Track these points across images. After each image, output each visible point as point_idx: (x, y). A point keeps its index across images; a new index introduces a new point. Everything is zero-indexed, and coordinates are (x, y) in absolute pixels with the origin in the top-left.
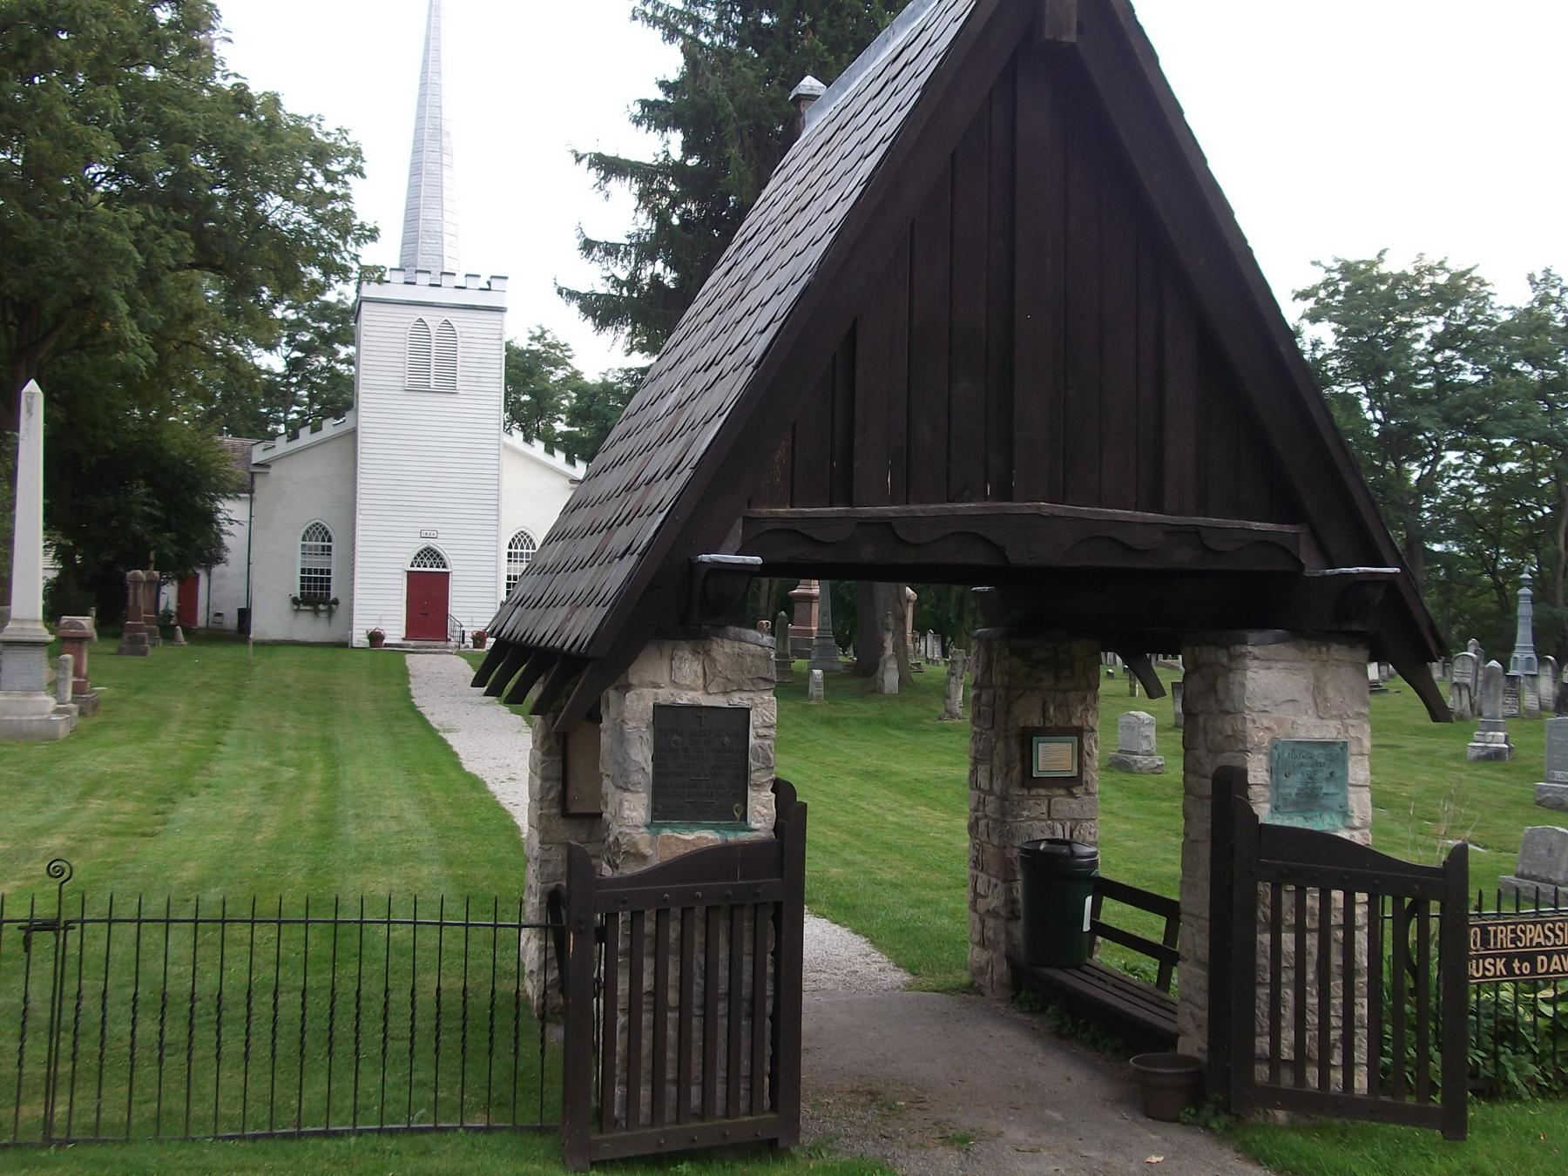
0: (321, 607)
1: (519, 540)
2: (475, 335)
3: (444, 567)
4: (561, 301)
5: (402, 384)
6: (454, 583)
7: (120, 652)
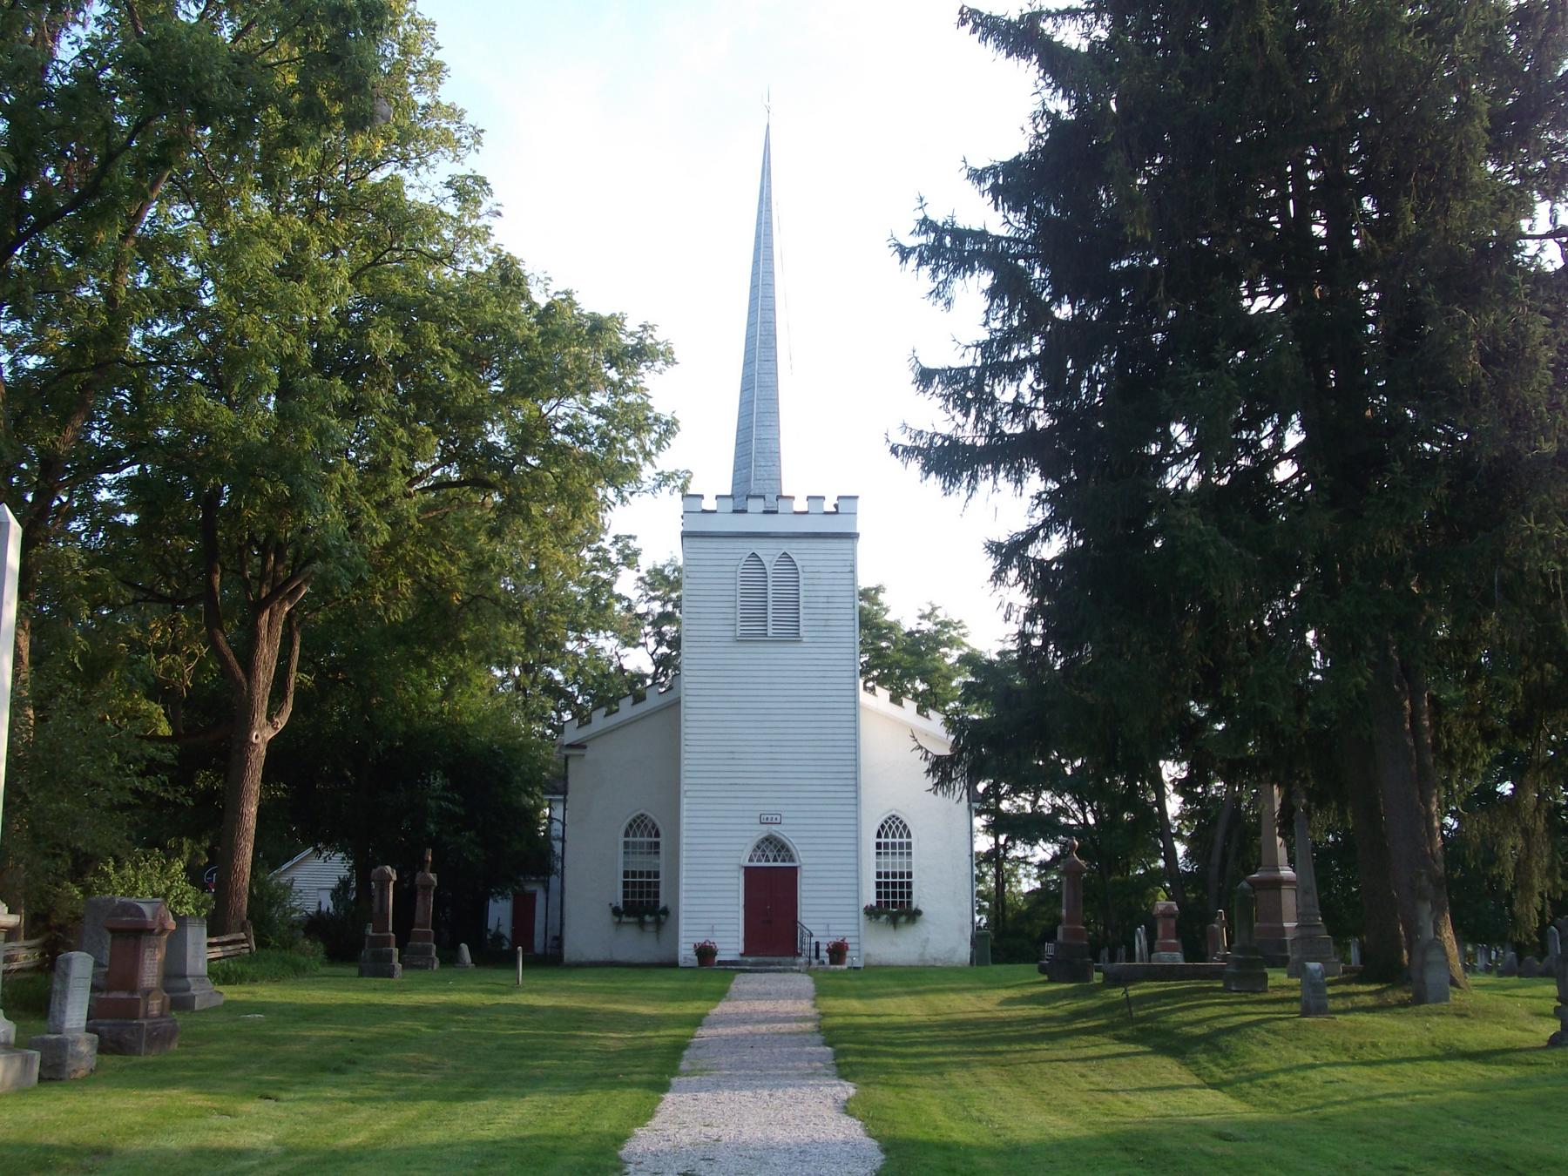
0: (648, 918)
1: (890, 827)
2: (821, 569)
4: (896, 462)
5: (732, 634)
7: (361, 974)
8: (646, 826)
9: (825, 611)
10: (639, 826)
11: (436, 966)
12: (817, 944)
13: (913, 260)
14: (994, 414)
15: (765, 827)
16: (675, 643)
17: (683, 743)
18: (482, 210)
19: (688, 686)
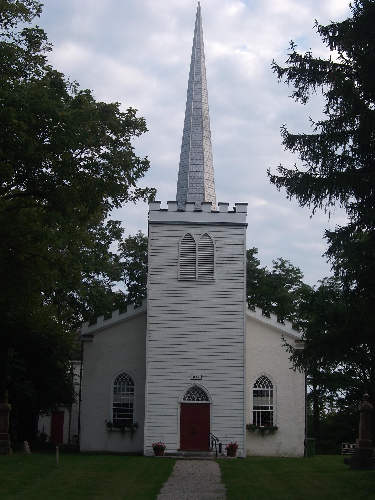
0: (126, 429)
1: (261, 382)
2: (226, 243)
4: (273, 187)
5: (176, 277)
6: (214, 411)
8: (126, 379)
9: (228, 265)
10: (122, 379)
11: (11, 453)
12: (221, 445)
13: (285, 76)
14: (332, 162)
15: (192, 382)
16: (143, 279)
17: (148, 335)
18: (41, 47)
19: (151, 305)
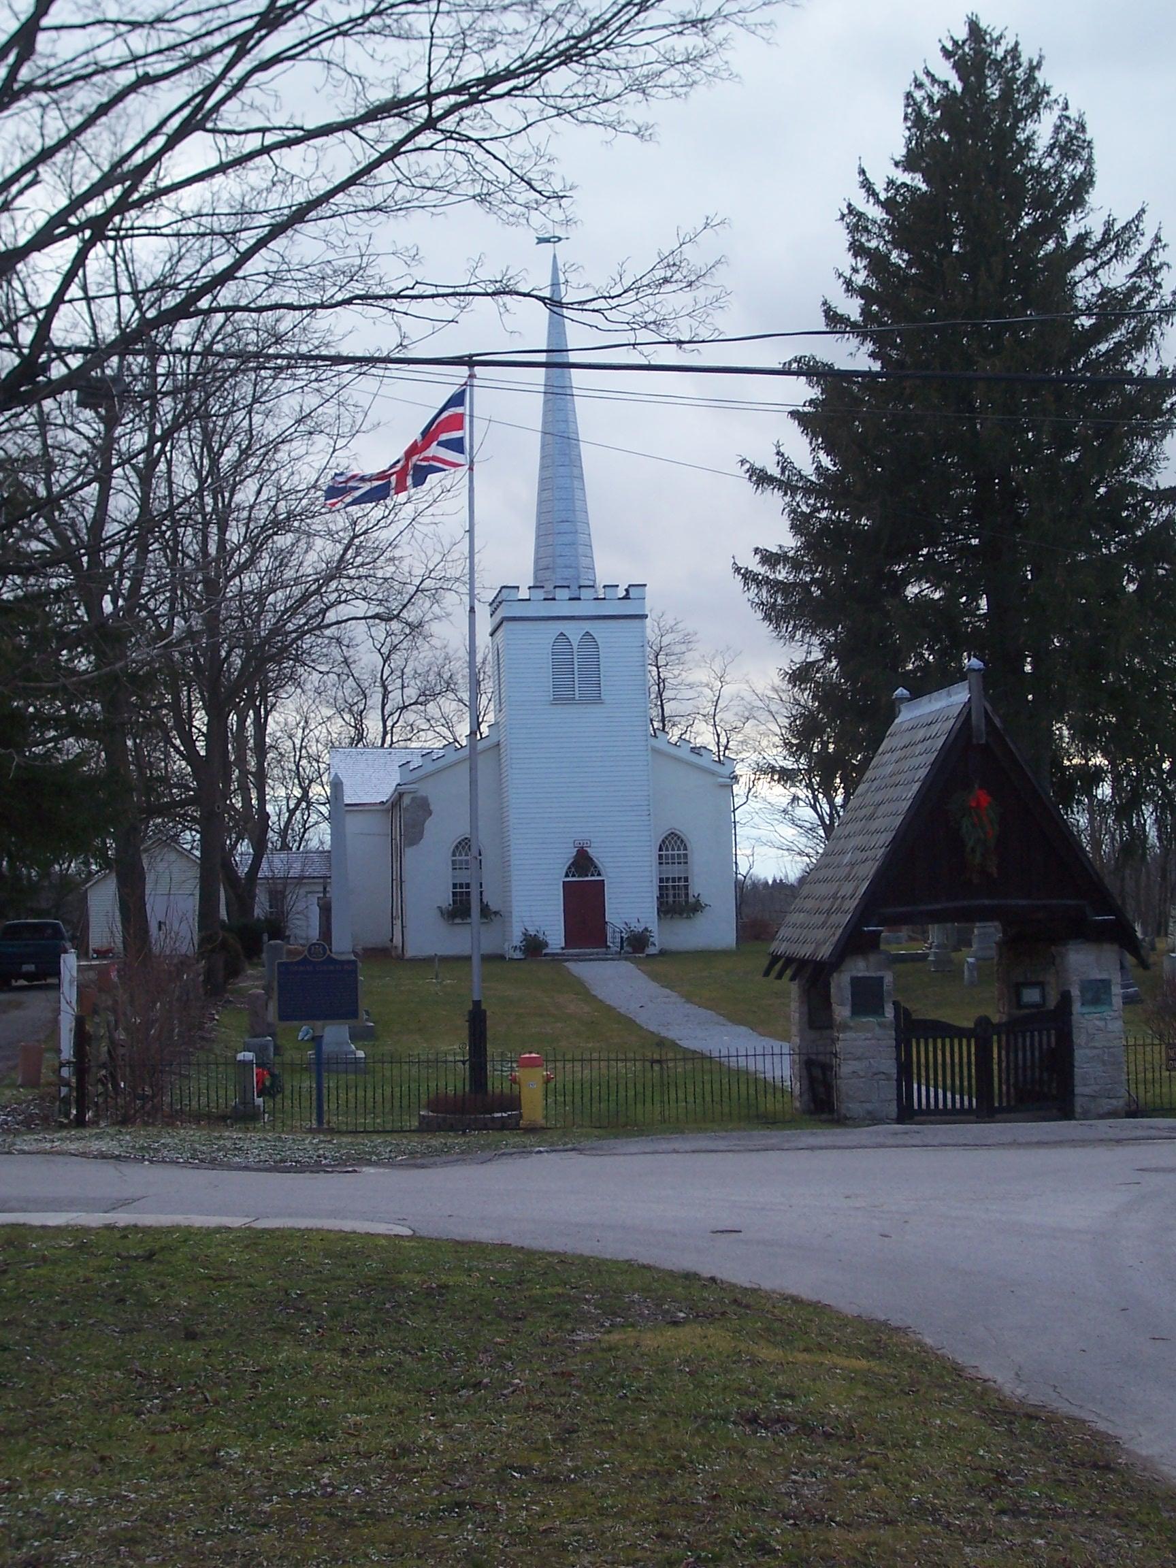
3: (599, 875)
